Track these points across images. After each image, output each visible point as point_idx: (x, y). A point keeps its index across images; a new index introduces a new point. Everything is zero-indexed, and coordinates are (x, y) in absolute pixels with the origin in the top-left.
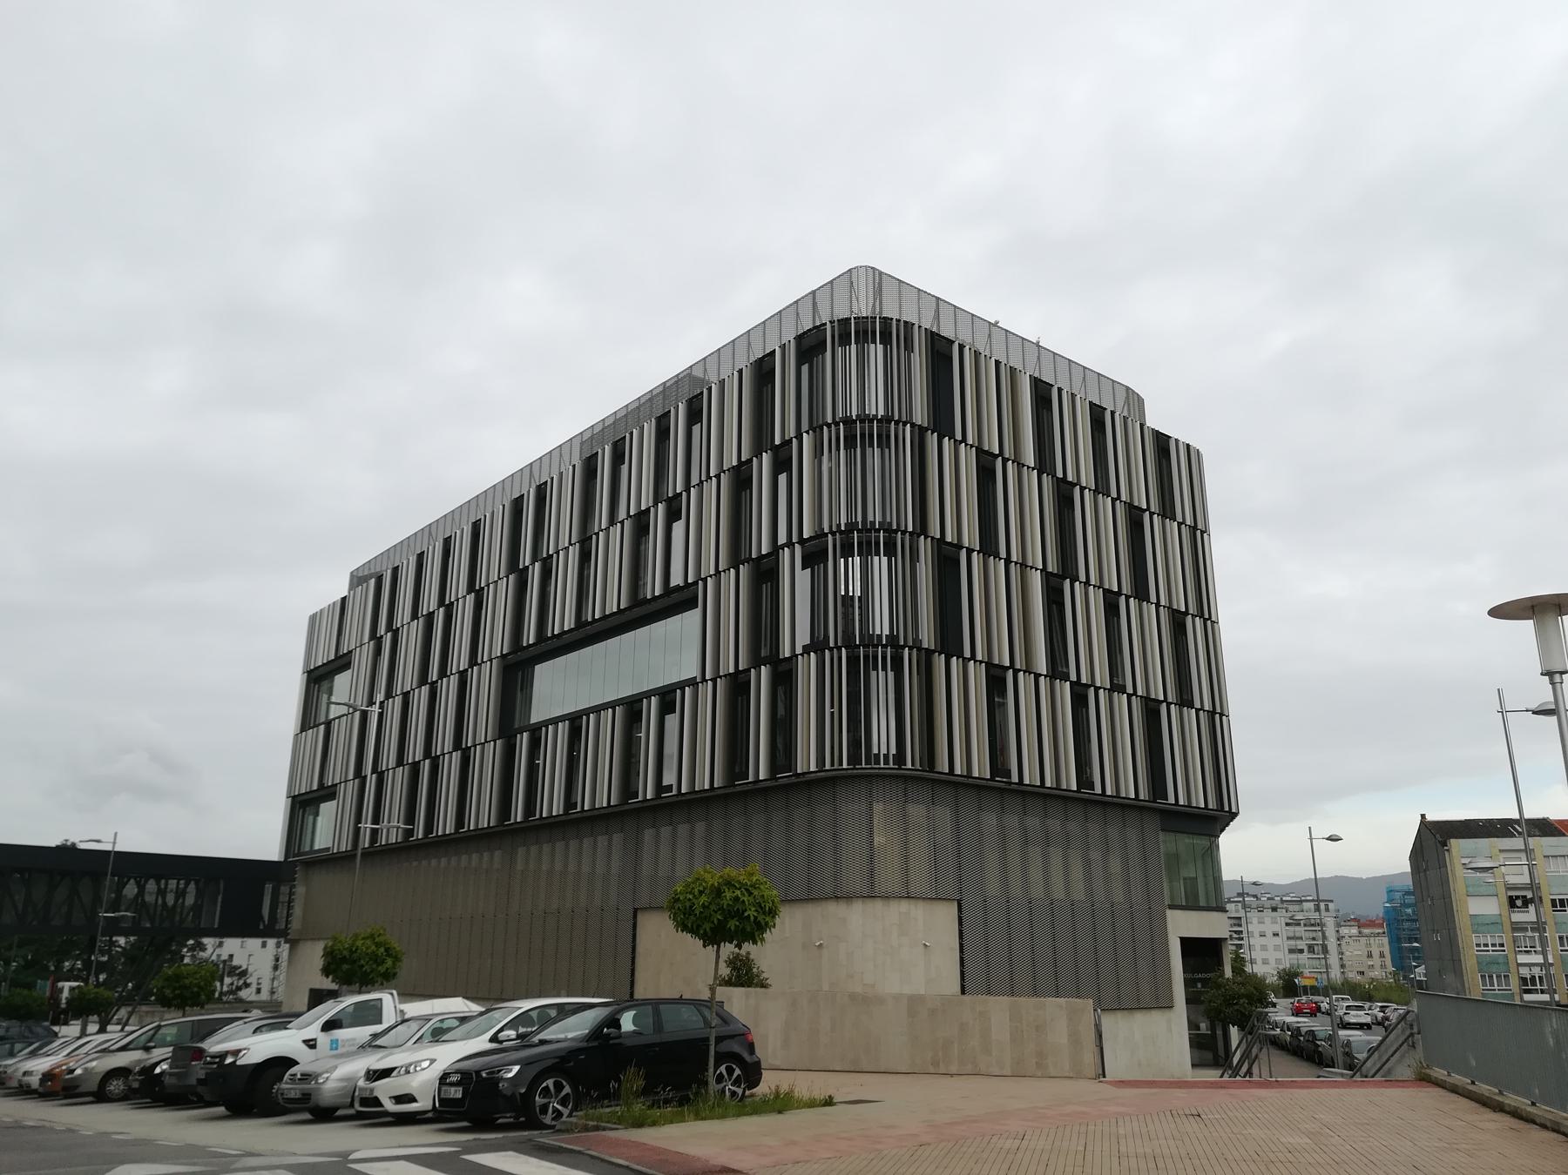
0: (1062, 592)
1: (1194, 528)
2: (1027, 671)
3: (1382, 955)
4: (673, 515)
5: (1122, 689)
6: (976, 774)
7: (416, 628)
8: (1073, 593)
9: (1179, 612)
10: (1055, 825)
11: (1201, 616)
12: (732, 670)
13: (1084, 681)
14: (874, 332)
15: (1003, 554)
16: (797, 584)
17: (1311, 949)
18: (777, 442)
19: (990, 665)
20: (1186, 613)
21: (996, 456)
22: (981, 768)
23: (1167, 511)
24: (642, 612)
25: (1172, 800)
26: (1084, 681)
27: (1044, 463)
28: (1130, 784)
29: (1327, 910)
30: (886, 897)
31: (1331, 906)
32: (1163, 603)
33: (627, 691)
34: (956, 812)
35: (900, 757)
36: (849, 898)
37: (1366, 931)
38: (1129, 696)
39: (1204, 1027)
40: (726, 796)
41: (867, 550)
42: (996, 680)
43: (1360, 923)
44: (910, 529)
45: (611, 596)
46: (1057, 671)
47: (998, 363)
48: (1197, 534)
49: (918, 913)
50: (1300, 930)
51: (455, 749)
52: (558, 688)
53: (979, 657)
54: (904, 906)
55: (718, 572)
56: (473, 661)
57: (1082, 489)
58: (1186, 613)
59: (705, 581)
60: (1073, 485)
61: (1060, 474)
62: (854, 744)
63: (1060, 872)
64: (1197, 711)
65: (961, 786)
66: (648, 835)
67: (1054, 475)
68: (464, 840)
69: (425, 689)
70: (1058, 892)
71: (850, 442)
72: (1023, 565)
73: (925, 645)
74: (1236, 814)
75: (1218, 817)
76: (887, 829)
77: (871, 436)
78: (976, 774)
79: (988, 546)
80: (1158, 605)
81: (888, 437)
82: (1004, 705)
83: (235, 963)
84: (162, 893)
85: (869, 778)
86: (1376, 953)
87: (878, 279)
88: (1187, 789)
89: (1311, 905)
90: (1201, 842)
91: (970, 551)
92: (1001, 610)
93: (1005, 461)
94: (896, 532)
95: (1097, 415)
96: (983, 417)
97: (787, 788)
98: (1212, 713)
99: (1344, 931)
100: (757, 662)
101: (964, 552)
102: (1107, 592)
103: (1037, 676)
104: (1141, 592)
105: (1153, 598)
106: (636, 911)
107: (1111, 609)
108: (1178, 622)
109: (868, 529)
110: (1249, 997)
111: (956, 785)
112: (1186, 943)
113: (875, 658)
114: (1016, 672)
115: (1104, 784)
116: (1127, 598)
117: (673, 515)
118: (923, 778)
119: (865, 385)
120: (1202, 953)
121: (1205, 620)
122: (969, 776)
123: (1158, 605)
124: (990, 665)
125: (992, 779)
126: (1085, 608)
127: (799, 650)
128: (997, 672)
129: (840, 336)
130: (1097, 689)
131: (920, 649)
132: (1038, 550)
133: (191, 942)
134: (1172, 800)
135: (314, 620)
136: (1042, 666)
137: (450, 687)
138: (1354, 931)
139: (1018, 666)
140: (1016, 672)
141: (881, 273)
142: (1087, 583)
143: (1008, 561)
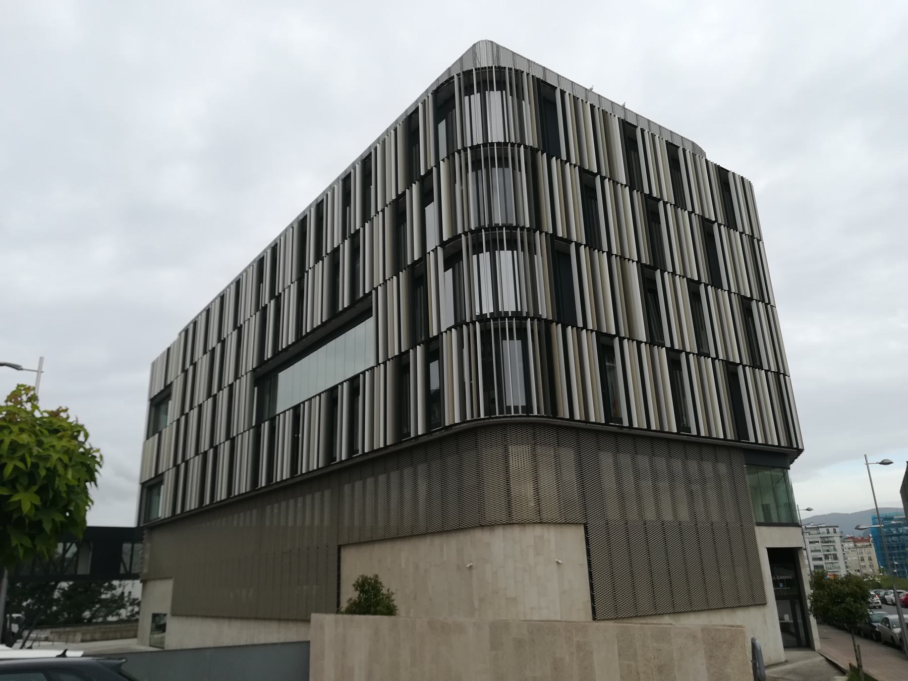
0: (654, 282)
1: (752, 237)
2: (631, 339)
3: (870, 559)
4: (426, 198)
5: (708, 355)
6: (593, 419)
7: (207, 358)
8: (663, 282)
9: (745, 297)
10: (661, 463)
11: (763, 301)
12: (396, 353)
13: (677, 347)
14: (491, 82)
15: (605, 248)
16: (441, 283)
17: (827, 557)
18: (422, 173)
19: (600, 334)
20: (751, 299)
21: (596, 175)
22: (596, 414)
23: (731, 223)
24: (339, 323)
25: (752, 440)
26: (677, 347)
27: (634, 182)
28: (720, 428)
29: (835, 532)
30: (522, 524)
31: (837, 529)
32: (733, 290)
33: (350, 375)
34: (579, 454)
35: (528, 408)
36: (492, 526)
37: (859, 544)
38: (713, 360)
39: (787, 618)
40: (398, 453)
41: (494, 246)
42: (587, 181)
43: (855, 540)
44: (528, 225)
45: (316, 314)
46: (655, 338)
47: (592, 107)
48: (754, 241)
49: (550, 535)
50: (818, 546)
51: (227, 440)
52: (300, 383)
53: (590, 327)
54: (538, 530)
55: (385, 281)
56: (237, 377)
57: (665, 204)
58: (751, 299)
59: (376, 289)
60: (658, 200)
61: (647, 191)
62: (489, 402)
63: (664, 499)
64: (766, 371)
65: (579, 432)
66: (347, 488)
67: (642, 192)
68: (234, 503)
69: (210, 400)
70: (668, 516)
71: (476, 166)
72: (622, 258)
73: (545, 317)
74: (799, 451)
75: (787, 452)
76: (528, 471)
77: (493, 159)
78: (593, 419)
79: (593, 242)
80: (729, 292)
81: (506, 159)
82: (613, 368)
83: (133, 596)
84: (65, 551)
85: (504, 426)
86: (866, 559)
87: (496, 49)
88: (764, 431)
89: (825, 530)
90: (777, 473)
91: (578, 245)
92: (605, 290)
93: (603, 179)
94: (516, 228)
95: (672, 149)
96: (582, 145)
97: (441, 440)
98: (777, 374)
99: (846, 545)
100: (413, 345)
101: (573, 246)
102: (690, 281)
103: (639, 343)
104: (716, 282)
105: (726, 287)
106: (339, 548)
107: (695, 297)
108: (746, 304)
109: (492, 228)
110: (853, 595)
111: (578, 430)
112: (771, 552)
113: (504, 330)
114: (621, 340)
115: (698, 427)
116: (706, 286)
117: (426, 198)
118: (548, 425)
119: (491, 119)
120: (785, 559)
121: (766, 305)
122: (587, 421)
123: (729, 292)
124: (600, 334)
125: (606, 424)
126: (674, 295)
127: (443, 329)
128: (604, 340)
129: (466, 88)
130: (687, 354)
131: (540, 319)
132: (634, 246)
133: (106, 584)
134: (752, 440)
135: (154, 365)
136: (642, 335)
137: (223, 396)
138: (852, 545)
139: (623, 335)
140: (621, 340)
141: (498, 46)
142: (674, 273)
143: (610, 254)
